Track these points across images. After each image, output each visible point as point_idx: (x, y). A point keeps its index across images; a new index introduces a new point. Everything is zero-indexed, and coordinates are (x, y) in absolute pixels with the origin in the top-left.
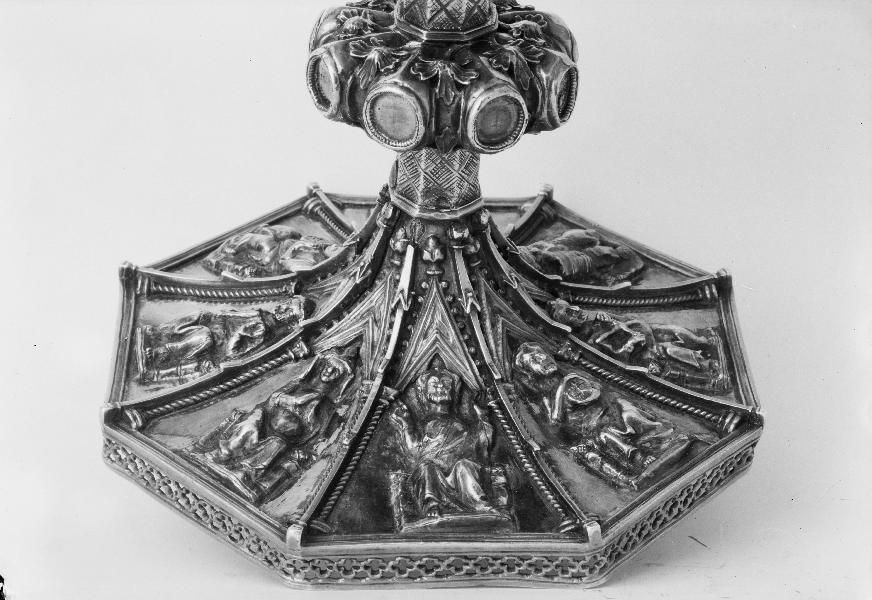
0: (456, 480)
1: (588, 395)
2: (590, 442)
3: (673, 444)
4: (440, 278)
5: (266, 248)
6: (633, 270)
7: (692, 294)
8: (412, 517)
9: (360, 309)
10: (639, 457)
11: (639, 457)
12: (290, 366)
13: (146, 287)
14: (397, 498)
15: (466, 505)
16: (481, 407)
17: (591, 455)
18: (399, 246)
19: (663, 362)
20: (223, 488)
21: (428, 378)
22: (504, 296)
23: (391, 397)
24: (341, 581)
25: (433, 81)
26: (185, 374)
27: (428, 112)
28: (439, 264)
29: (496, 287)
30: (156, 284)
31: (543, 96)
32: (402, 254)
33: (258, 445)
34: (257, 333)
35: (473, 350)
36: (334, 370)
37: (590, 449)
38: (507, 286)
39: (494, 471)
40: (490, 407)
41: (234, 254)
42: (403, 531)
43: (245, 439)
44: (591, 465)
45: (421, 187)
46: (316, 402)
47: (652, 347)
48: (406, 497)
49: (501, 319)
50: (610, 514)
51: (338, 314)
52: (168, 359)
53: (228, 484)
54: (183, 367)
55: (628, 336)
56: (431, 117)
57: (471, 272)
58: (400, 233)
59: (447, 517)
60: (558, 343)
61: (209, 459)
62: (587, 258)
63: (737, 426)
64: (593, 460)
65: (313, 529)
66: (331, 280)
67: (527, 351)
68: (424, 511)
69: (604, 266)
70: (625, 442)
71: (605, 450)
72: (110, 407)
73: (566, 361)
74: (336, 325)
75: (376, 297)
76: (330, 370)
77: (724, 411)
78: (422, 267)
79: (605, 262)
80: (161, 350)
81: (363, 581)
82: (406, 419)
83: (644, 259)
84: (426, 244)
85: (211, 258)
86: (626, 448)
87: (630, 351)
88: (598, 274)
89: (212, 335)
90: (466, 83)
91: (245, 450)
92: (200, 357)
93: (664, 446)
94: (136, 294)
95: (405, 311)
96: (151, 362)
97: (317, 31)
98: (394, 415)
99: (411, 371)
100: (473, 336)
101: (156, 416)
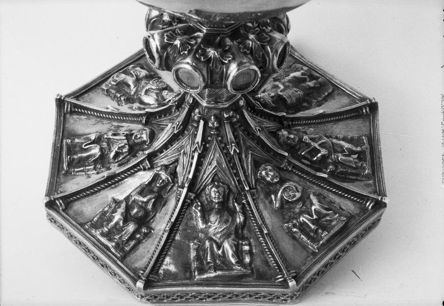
0: (223, 252)
1: (294, 196)
2: (295, 222)
3: (338, 223)
4: (218, 135)
5: (132, 86)
6: (326, 94)
7: (356, 112)
8: (202, 271)
9: (176, 146)
10: (320, 231)
11: (320, 231)
12: (141, 173)
13: (69, 109)
14: (194, 258)
15: (226, 265)
16: (239, 204)
17: (295, 230)
18: (196, 118)
19: (336, 164)
20: (105, 250)
21: (212, 188)
22: (253, 140)
23: (192, 198)
24: (165, 301)
25: (209, 60)
26: (88, 171)
27: (206, 76)
28: (217, 129)
29: (248, 134)
30: (74, 107)
31: (269, 62)
32: (198, 122)
33: (123, 227)
34: (125, 150)
35: (235, 171)
36: (163, 181)
37: (294, 226)
38: (254, 134)
39: (244, 243)
40: (243, 204)
41: (115, 85)
42: (196, 279)
43: (117, 223)
44: (295, 235)
45: (206, 93)
46: (153, 200)
47: (331, 156)
48: (198, 258)
49: (250, 152)
50: (303, 268)
51: (166, 146)
52: (79, 162)
53: (107, 248)
54: (87, 168)
55: (319, 151)
56: (208, 79)
57: (234, 131)
58: (197, 111)
59: (219, 273)
60: (280, 160)
61: (97, 233)
62: (300, 93)
63: (372, 207)
64: (296, 232)
65: (150, 280)
66: (164, 120)
67: (265, 169)
68: (207, 268)
69: (312, 93)
70: (313, 224)
71: (303, 227)
72: (48, 199)
73: (285, 170)
74: (165, 152)
75: (184, 141)
76: (161, 181)
77: (366, 198)
78: (208, 130)
79: (311, 91)
80: (75, 157)
81: (176, 301)
82: (200, 211)
83: (333, 85)
84: (210, 119)
85: (104, 86)
86: (313, 227)
87: (319, 159)
88: (307, 98)
89: (101, 149)
90: (226, 62)
91: (117, 229)
92: (95, 162)
93: (334, 223)
94: (64, 113)
95: (199, 153)
96: (70, 164)
97: (149, 15)
98: (194, 208)
99: (203, 182)
100: (235, 164)
101: (72, 201)
